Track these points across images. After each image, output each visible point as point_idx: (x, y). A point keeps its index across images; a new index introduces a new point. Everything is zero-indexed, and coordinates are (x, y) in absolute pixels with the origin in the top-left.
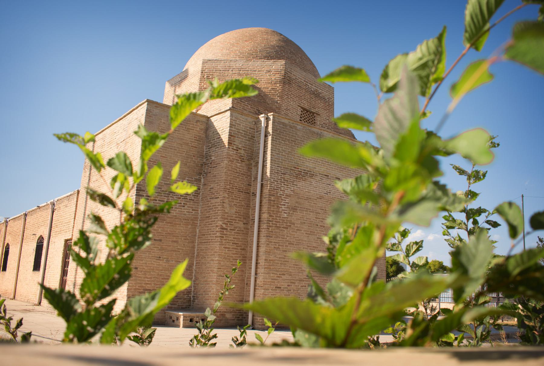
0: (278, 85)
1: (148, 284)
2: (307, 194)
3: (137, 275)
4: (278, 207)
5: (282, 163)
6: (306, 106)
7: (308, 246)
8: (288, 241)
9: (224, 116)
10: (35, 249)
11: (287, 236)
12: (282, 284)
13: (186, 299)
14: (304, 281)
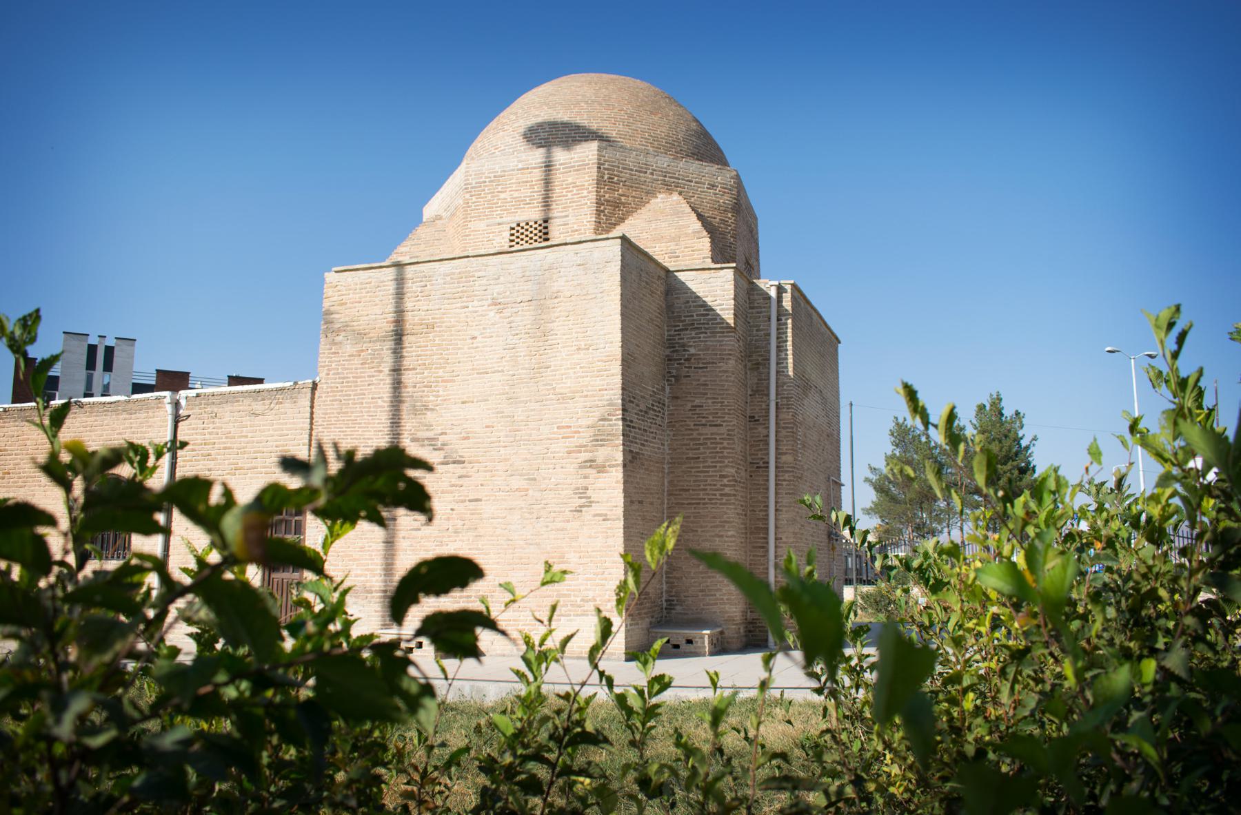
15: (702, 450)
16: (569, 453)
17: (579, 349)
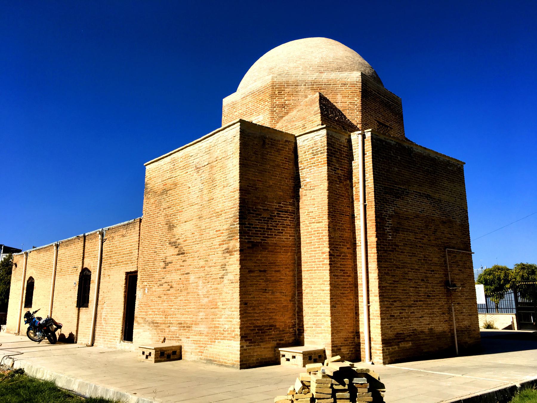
0: (356, 99)
1: (257, 320)
2: (406, 213)
3: (247, 311)
4: (383, 229)
5: (383, 182)
6: (382, 121)
7: (412, 269)
8: (395, 265)
9: (317, 134)
10: (77, 283)
11: (394, 260)
12: (395, 311)
13: (292, 333)
14: (412, 307)
15: (313, 238)
16: (220, 245)
17: (224, 187)
